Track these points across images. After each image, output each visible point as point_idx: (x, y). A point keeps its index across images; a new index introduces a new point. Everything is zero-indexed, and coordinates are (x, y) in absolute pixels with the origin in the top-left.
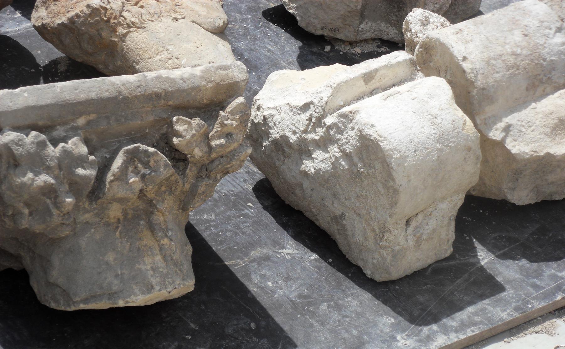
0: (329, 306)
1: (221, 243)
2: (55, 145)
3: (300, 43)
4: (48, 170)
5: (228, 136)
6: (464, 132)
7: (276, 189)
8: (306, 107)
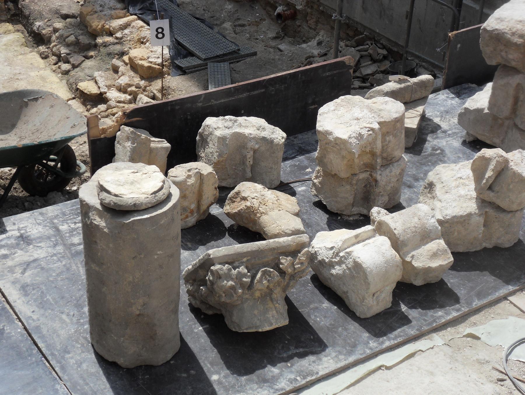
0: (342, 329)
1: (298, 302)
2: (235, 269)
3: (327, 216)
4: (232, 279)
5: (302, 263)
6: (396, 259)
7: (320, 279)
8: (332, 248)
